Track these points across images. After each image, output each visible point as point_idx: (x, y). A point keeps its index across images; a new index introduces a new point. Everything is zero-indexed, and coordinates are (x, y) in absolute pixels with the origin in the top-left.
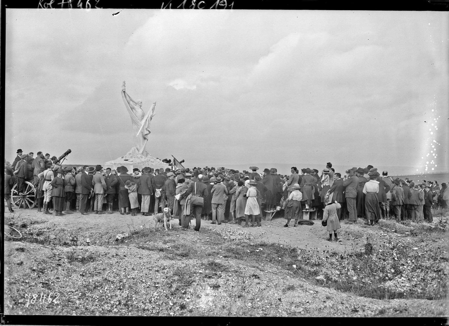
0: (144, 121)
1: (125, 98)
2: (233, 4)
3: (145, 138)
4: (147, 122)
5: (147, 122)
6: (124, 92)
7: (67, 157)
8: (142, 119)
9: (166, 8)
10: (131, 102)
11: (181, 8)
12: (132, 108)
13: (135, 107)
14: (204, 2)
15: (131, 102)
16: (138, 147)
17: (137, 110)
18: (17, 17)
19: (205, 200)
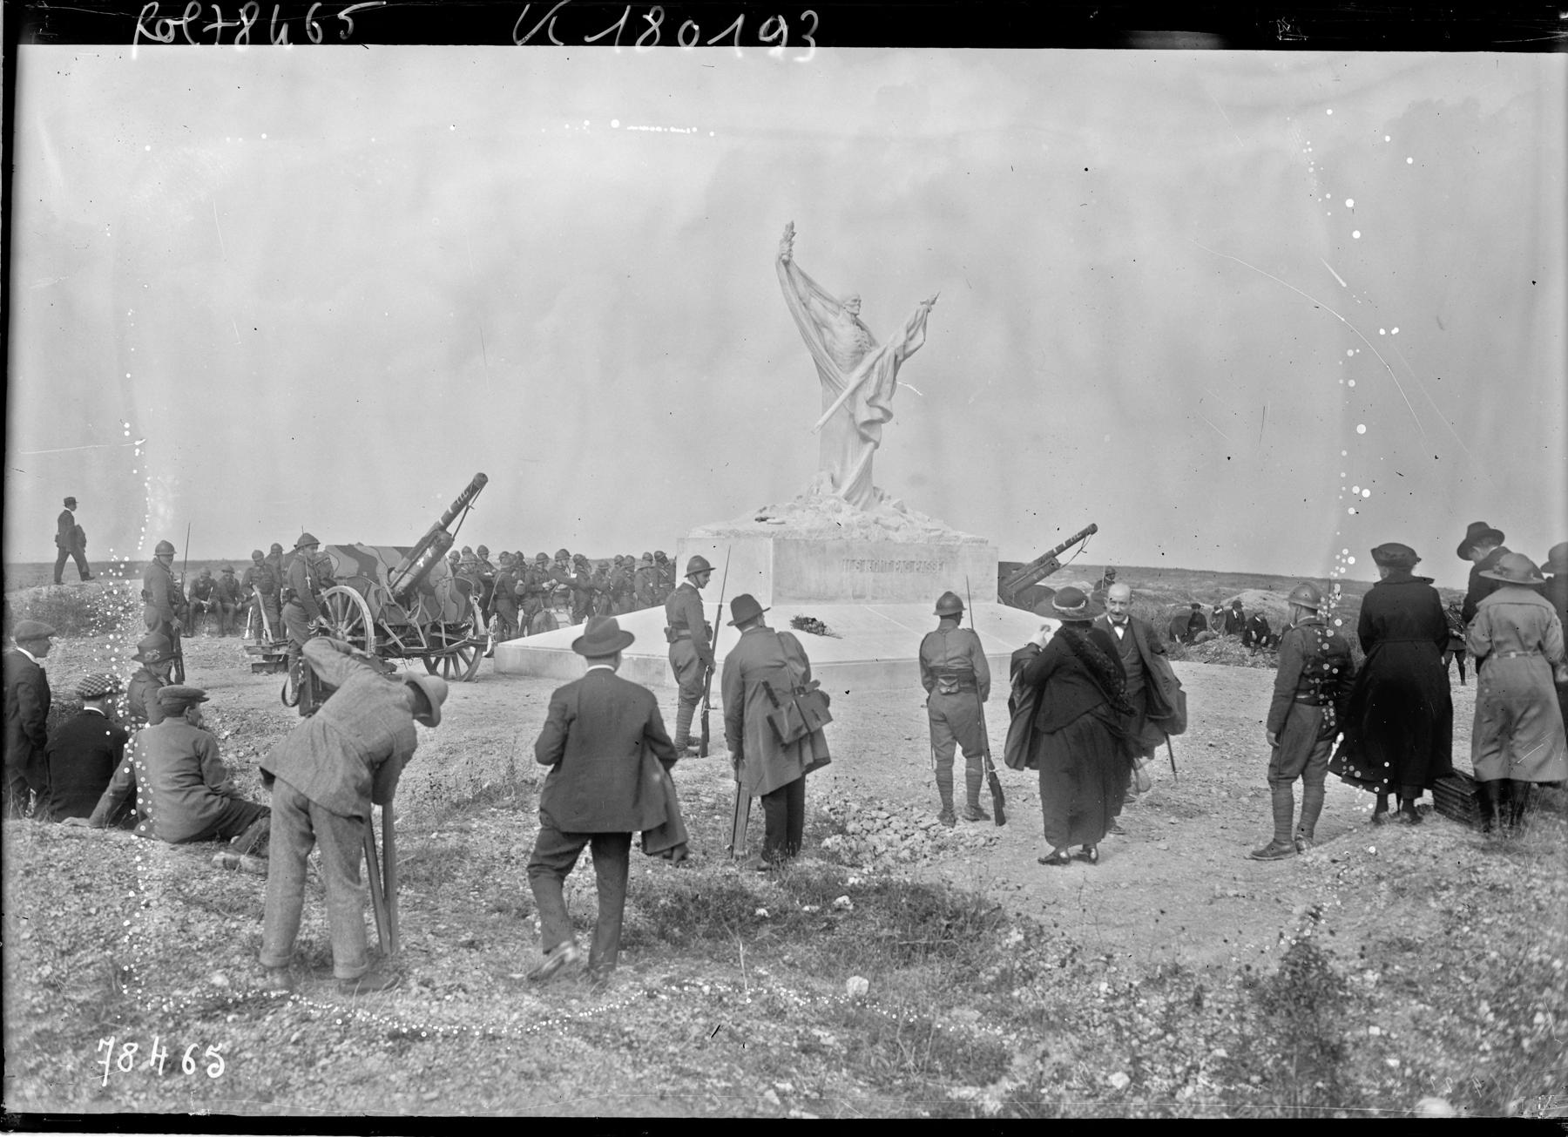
0: (861, 370)
1: (788, 287)
2: (740, 21)
3: (865, 439)
4: (874, 378)
5: (874, 378)
6: (786, 263)
7: (479, 502)
8: (856, 363)
9: (528, 43)
10: (816, 303)
11: (608, 41)
12: (820, 325)
13: (831, 318)
14: (318, 5)
15: (816, 303)
16: (837, 473)
17: (836, 329)
18: (57, 75)
19: (1368, 663)
